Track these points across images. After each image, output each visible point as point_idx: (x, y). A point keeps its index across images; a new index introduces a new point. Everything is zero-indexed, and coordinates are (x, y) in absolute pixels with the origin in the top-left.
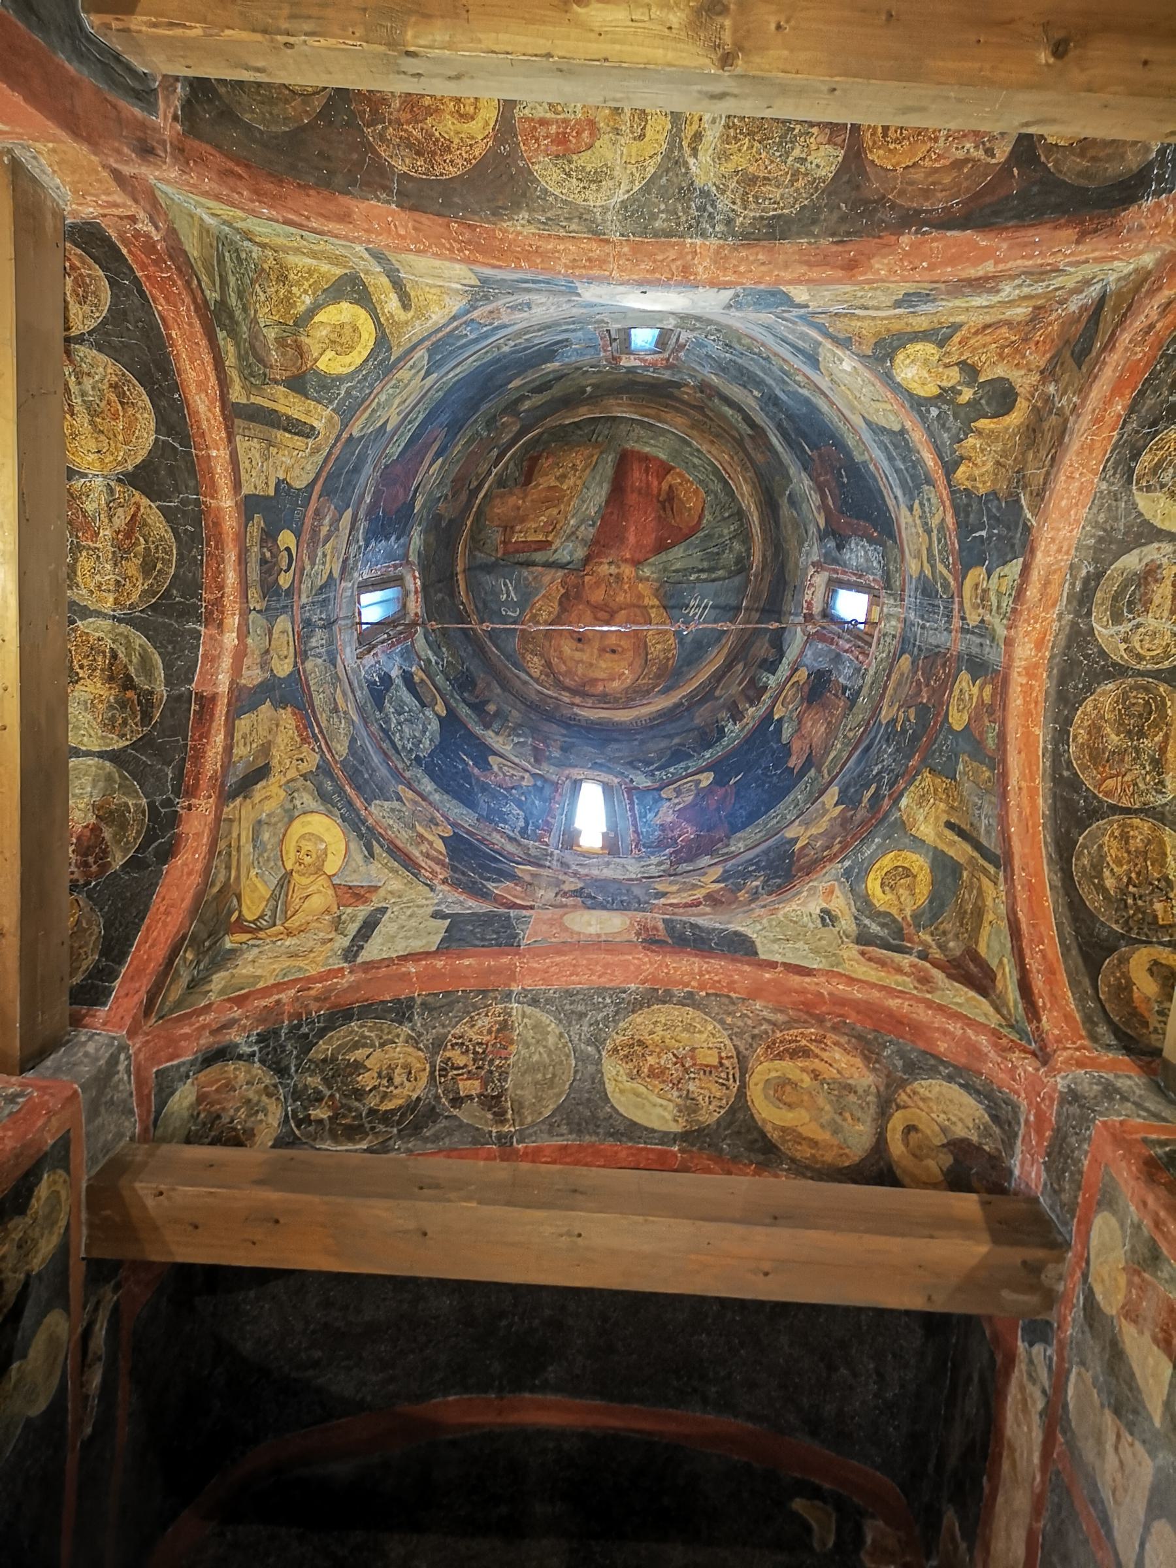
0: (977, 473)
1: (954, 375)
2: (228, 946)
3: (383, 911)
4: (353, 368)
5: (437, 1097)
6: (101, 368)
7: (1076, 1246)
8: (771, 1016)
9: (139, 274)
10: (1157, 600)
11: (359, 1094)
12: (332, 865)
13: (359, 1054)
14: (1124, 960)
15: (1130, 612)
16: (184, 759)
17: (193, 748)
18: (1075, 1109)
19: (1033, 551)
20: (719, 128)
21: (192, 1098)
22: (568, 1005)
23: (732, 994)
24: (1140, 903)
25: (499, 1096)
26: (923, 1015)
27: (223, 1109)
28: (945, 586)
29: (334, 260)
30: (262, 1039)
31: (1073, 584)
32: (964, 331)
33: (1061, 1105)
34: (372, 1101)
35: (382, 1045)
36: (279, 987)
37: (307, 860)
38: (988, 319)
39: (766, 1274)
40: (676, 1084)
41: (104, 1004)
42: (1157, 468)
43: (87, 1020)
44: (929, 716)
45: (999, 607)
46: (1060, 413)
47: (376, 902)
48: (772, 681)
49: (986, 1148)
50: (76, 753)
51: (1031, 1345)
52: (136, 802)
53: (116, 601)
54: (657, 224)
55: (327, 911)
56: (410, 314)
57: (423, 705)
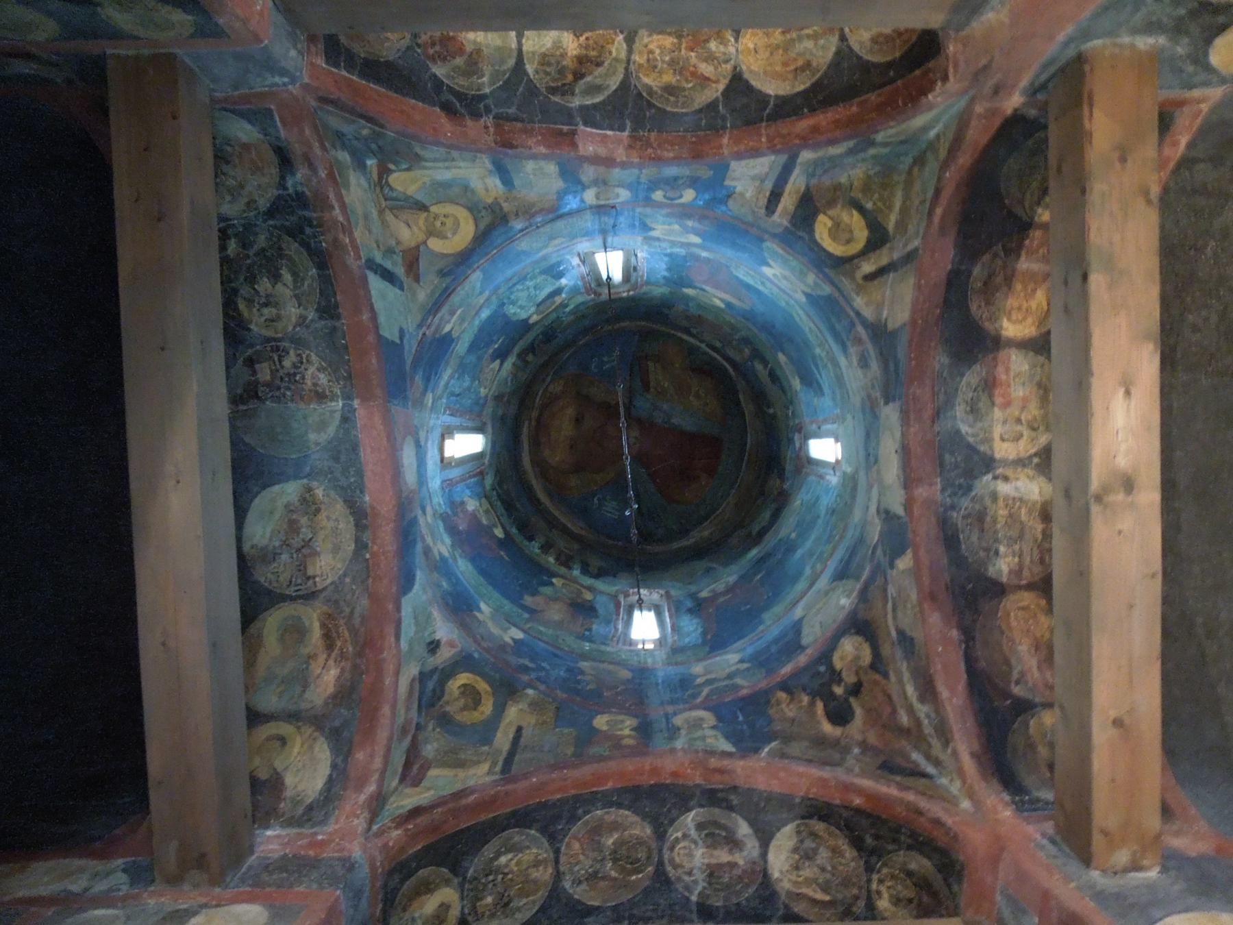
0: (784, 706)
1: (850, 678)
2: (369, 162)
3: (402, 288)
4: (819, 241)
5: (252, 346)
6: (822, 52)
7: (229, 893)
8: (357, 615)
9: (899, 83)
10: (716, 853)
11: (252, 280)
12: (435, 244)
13: (287, 277)
14: (447, 882)
15: (706, 835)
16: (522, 121)
17: (533, 129)
18: (340, 872)
19: (743, 757)
20: (1013, 494)
21: (244, 138)
22: (345, 451)
23: (371, 580)
24: (490, 886)
25: (258, 398)
26: (382, 735)
27: (235, 166)
28: (694, 696)
29: (901, 225)
30: (300, 196)
31: (722, 791)
32: (884, 682)
33: (339, 859)
34: (245, 291)
35: (296, 296)
36: (343, 206)
37: (438, 224)
38: (895, 698)
39: (164, 644)
40: (286, 544)
41: (327, 63)
42: (814, 835)
43: (313, 49)
44: (597, 699)
45: (695, 739)
46: (843, 759)
47: (407, 281)
48: (576, 573)
49: (282, 805)
50: (520, 36)
51: (124, 871)
52: (486, 83)
53: (641, 66)
54: (947, 457)
55: (398, 243)
56: (861, 282)
57: (538, 305)
